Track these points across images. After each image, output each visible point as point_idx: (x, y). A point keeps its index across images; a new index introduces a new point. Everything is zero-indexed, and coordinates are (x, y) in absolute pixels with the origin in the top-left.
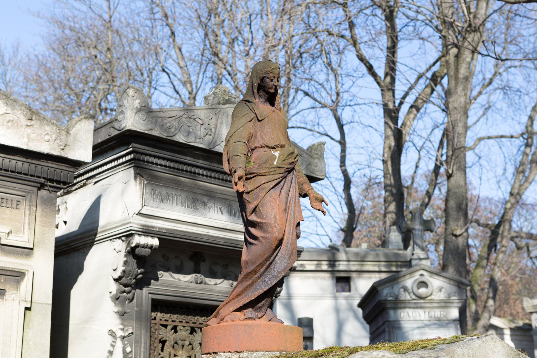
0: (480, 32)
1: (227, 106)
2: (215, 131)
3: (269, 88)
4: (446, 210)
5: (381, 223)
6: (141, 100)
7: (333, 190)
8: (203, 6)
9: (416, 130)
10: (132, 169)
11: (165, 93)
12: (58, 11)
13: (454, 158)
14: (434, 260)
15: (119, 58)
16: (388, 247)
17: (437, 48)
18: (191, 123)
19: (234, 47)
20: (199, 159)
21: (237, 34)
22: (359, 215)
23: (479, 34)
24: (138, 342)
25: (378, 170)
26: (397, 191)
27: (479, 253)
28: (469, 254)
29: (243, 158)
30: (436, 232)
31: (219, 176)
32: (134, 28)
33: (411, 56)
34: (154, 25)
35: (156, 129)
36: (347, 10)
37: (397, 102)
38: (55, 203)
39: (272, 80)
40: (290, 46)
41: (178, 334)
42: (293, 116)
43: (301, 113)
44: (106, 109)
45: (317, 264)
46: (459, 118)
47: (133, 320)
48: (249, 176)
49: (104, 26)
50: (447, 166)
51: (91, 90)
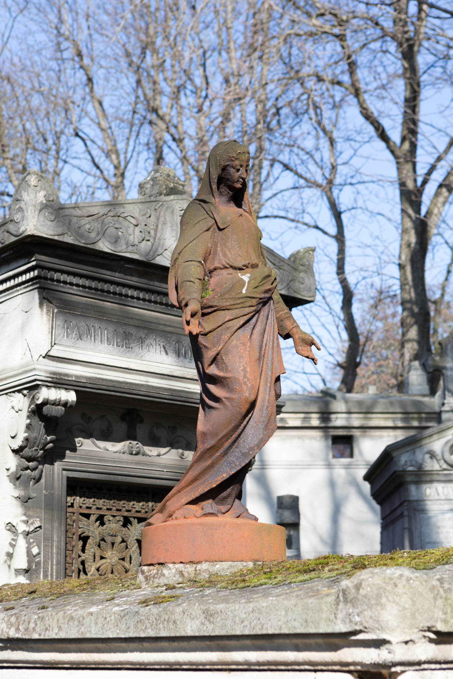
1: (172, 197)
2: (156, 235)
3: (234, 182)
5: (397, 354)
6: (47, 192)
7: (327, 308)
8: (133, 40)
10: (36, 292)
11: (79, 169)
15: (11, 118)
18: (120, 223)
19: (179, 99)
20: (132, 276)
21: (184, 78)
24: (48, 539)
25: (392, 278)
29: (198, 285)
32: (32, 72)
33: (441, 112)
34: (62, 68)
36: (345, 44)
37: (420, 180)
39: (238, 170)
41: (105, 526)
42: (267, 200)
43: (279, 196)
45: (305, 418)
47: (41, 508)
48: (207, 311)
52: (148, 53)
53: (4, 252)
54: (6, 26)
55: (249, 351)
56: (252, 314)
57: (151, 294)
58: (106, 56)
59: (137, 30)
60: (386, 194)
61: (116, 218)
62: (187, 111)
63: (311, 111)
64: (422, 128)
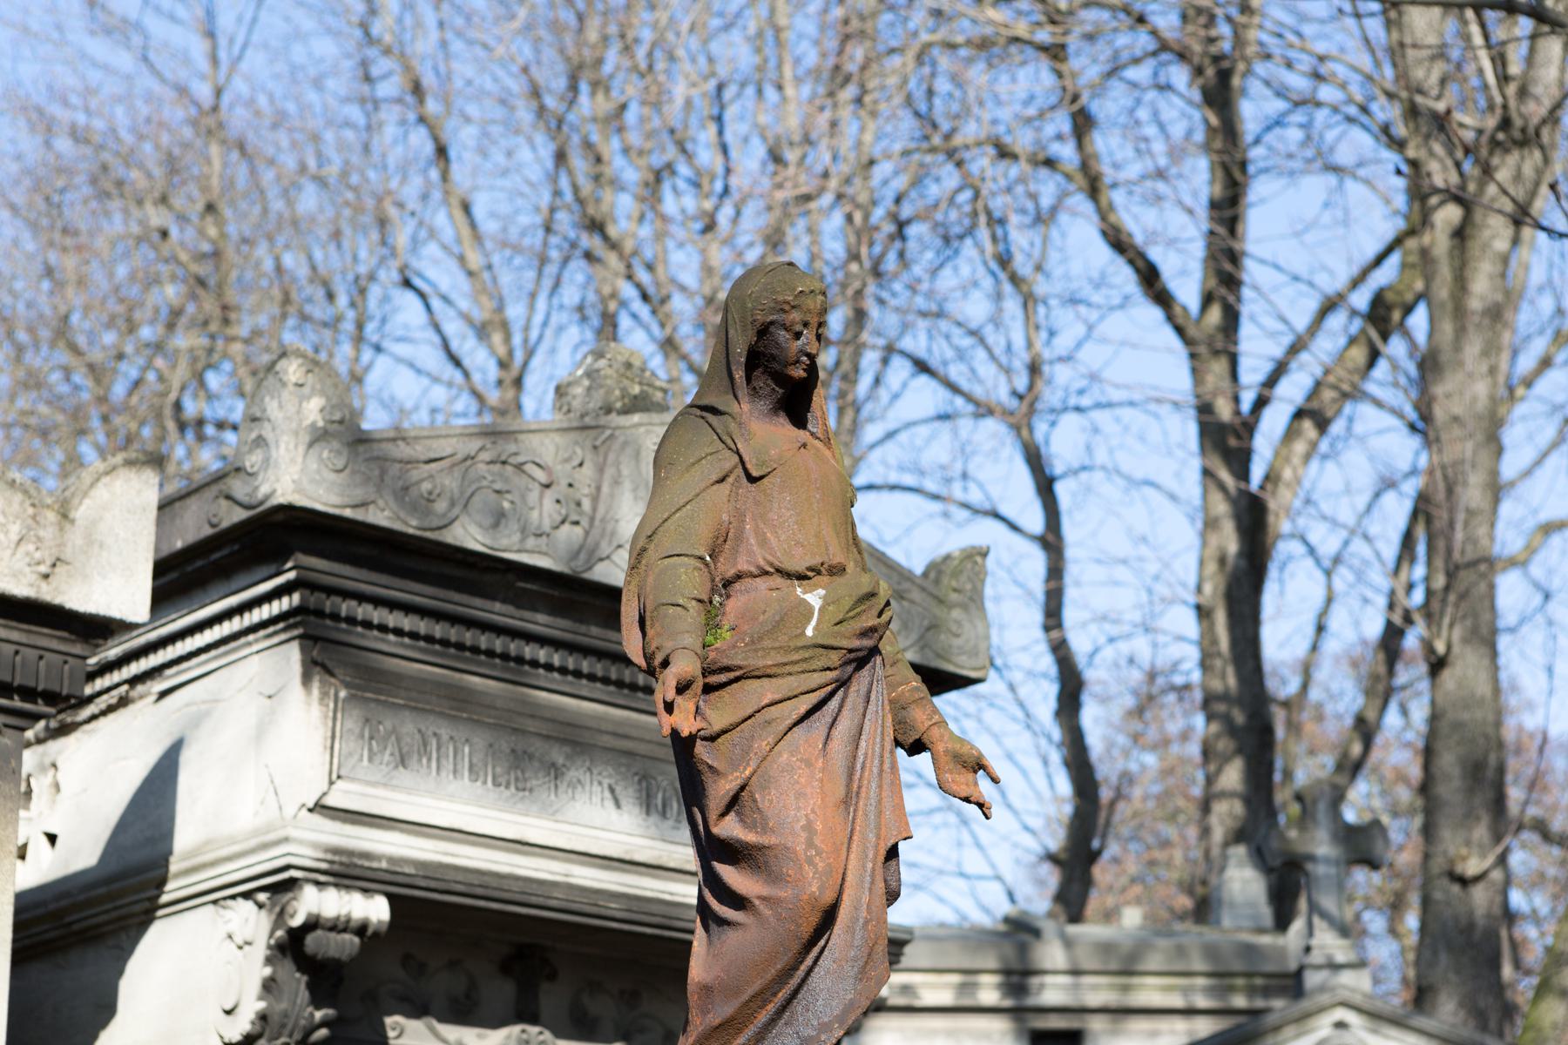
0: (1542, 148)
1: (636, 418)
2: (594, 509)
3: (787, 364)
4: (1425, 788)
5: (1192, 833)
6: (328, 399)
7: (1020, 714)
8: (549, 53)
9: (1315, 497)
11: (412, 365)
12: (28, 71)
13: (1452, 598)
14: (1383, 968)
15: (245, 241)
16: (1218, 922)
17: (1387, 201)
18: (506, 480)
20: (535, 609)
21: (671, 153)
22: (1112, 804)
23: (1537, 154)
25: (1180, 643)
26: (1249, 718)
27: (1549, 941)
28: (1515, 946)
30: (1391, 865)
31: (606, 669)
35: (381, 503)
36: (1064, 68)
37: (1247, 399)
38: (16, 772)
39: (798, 335)
40: (863, 198)
42: (872, 446)
43: (903, 437)
44: (200, 422)
46: (1469, 454)
48: (716, 679)
49: (194, 123)
50: (1429, 626)
51: (148, 352)
52: (584, 87)
53: (219, 548)
54: (240, 19)
55: (822, 780)
56: (829, 688)
57: (580, 656)
58: (481, 95)
59: (556, 27)
60: (1165, 433)
61: (497, 467)
62: (678, 232)
63: (983, 233)
64: (1253, 271)
